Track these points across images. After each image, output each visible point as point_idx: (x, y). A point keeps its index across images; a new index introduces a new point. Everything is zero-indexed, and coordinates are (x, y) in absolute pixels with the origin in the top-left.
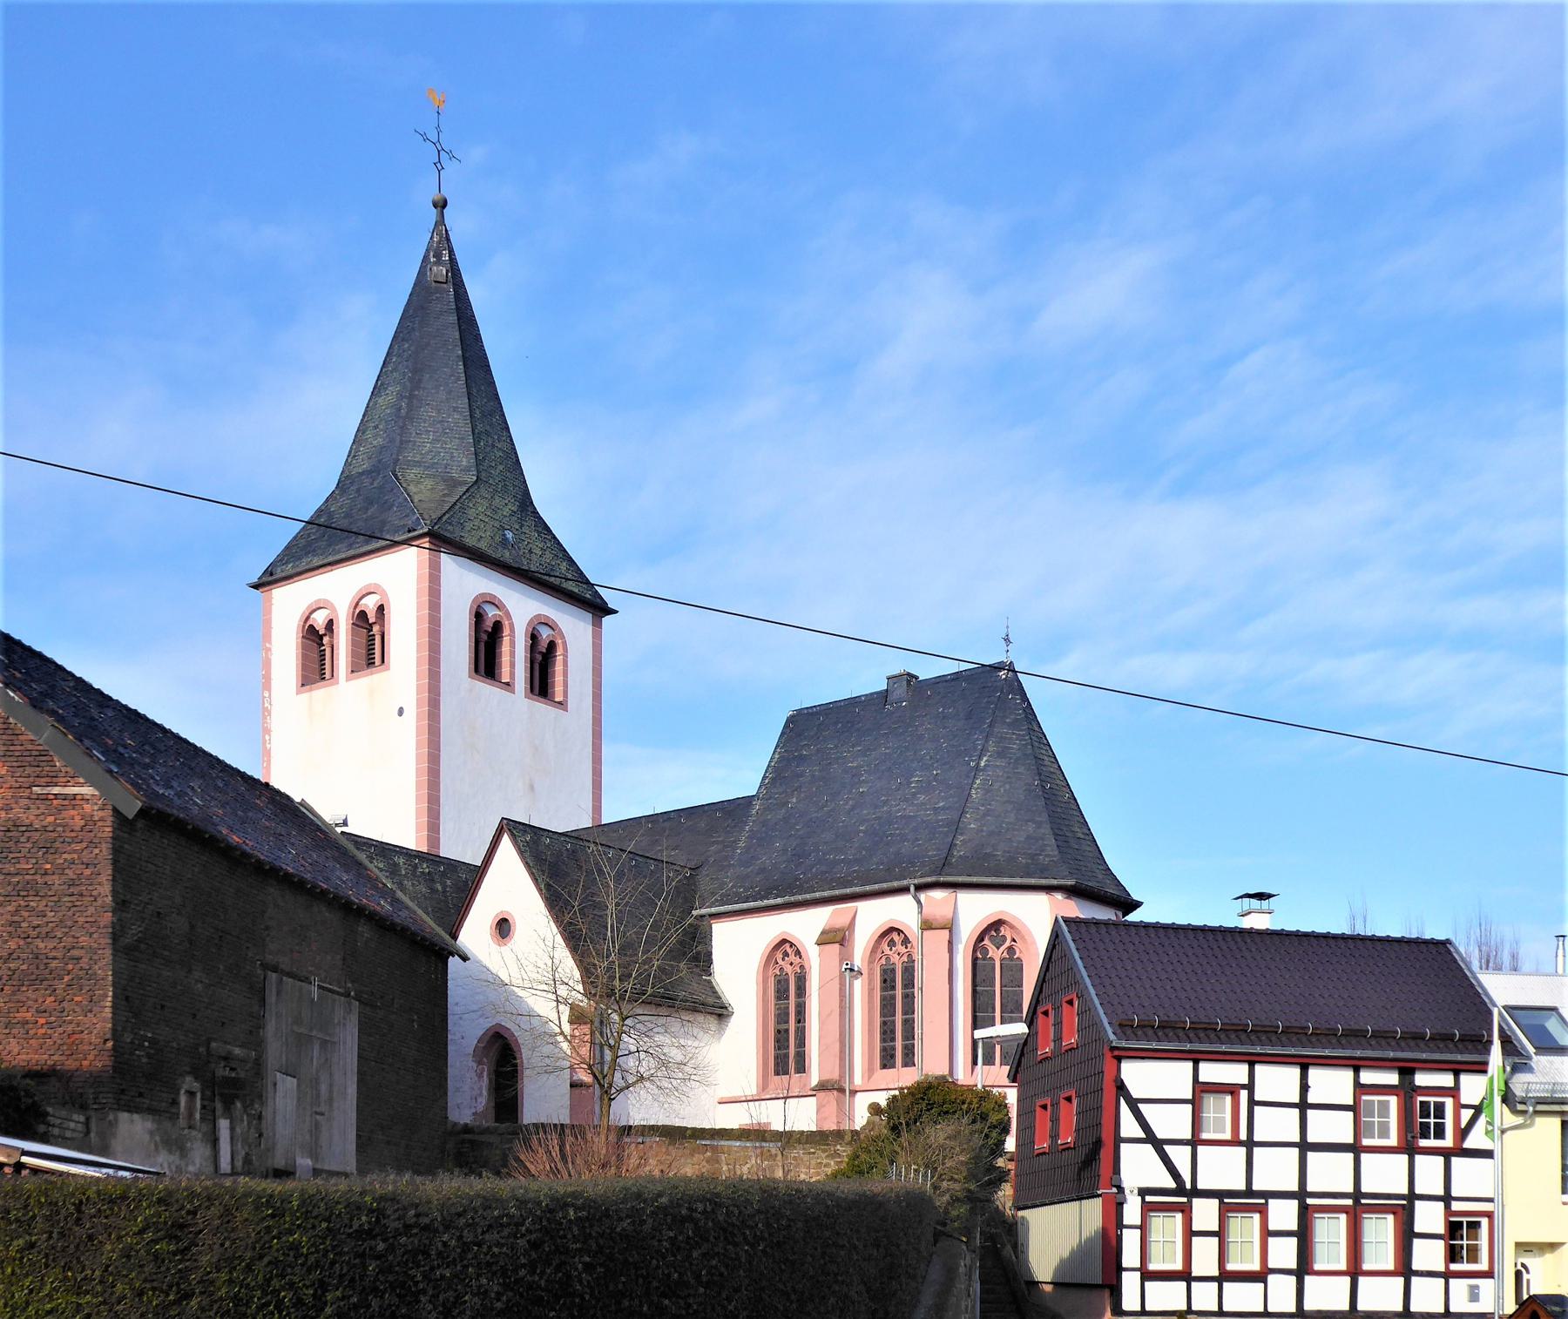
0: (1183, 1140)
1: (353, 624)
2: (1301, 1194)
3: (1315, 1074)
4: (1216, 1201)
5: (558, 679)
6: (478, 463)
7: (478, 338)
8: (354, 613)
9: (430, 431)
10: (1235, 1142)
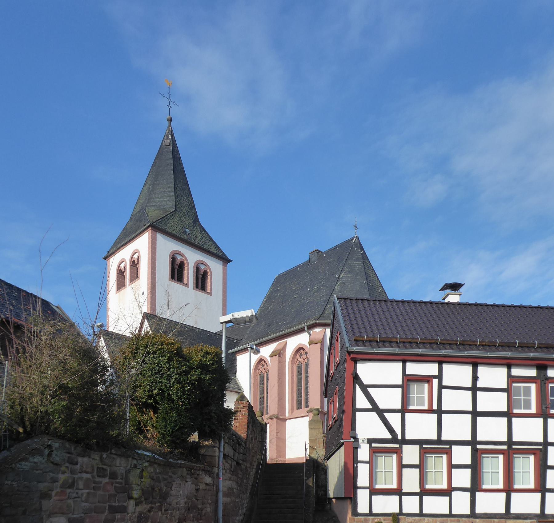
0: (396, 409)
1: (131, 265)
2: (473, 442)
3: (482, 370)
4: (418, 447)
5: (209, 284)
6: (176, 205)
7: (181, 164)
8: (131, 261)
9: (159, 195)
10: (430, 411)
